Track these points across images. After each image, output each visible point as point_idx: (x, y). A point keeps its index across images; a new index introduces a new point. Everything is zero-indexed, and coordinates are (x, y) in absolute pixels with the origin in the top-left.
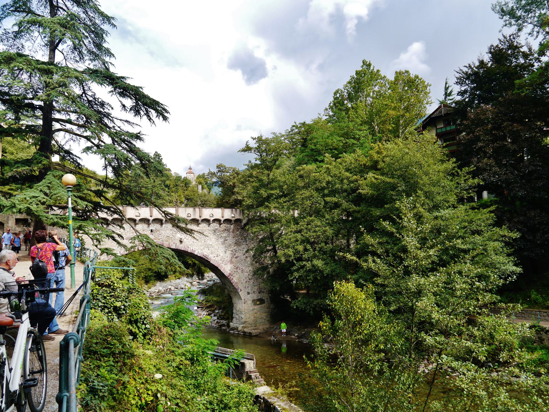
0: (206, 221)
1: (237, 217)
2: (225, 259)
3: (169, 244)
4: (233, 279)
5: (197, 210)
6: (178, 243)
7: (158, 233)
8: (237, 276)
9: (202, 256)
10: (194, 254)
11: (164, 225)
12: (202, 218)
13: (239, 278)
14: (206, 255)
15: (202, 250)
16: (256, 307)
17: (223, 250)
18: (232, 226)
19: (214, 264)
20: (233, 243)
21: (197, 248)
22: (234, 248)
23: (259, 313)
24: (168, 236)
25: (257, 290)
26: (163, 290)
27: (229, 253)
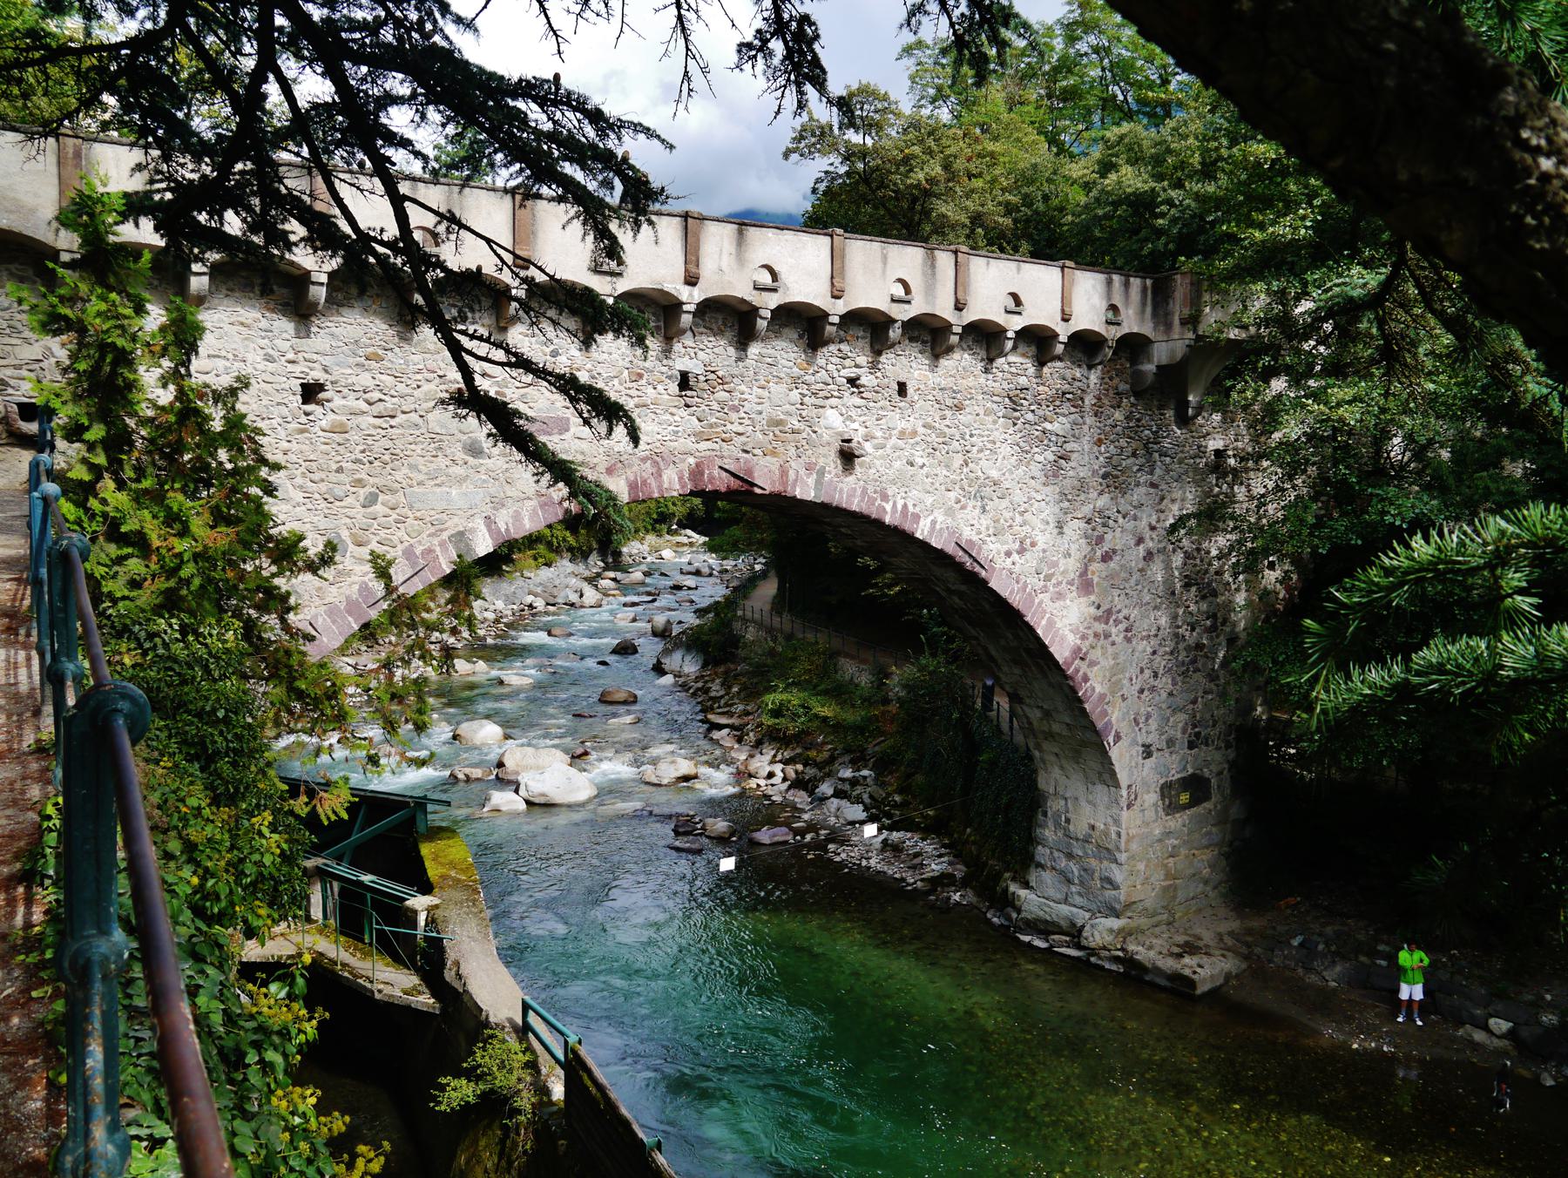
0: (985, 337)
1: (1133, 322)
2: (1055, 565)
3: (784, 473)
4: (1086, 679)
5: (944, 259)
6: (832, 464)
7: (722, 395)
8: (1107, 663)
9: (950, 549)
10: (878, 523)
11: (754, 349)
12: (970, 316)
13: (1116, 669)
14: (970, 542)
15: (949, 512)
16: (1177, 822)
17: (1049, 512)
18: (1094, 377)
19: (1004, 593)
20: (1094, 472)
21: (929, 500)
22: (1100, 503)
23: (1183, 851)
24: (779, 423)
25: (1184, 731)
26: (510, 613)
27: (1075, 528)
